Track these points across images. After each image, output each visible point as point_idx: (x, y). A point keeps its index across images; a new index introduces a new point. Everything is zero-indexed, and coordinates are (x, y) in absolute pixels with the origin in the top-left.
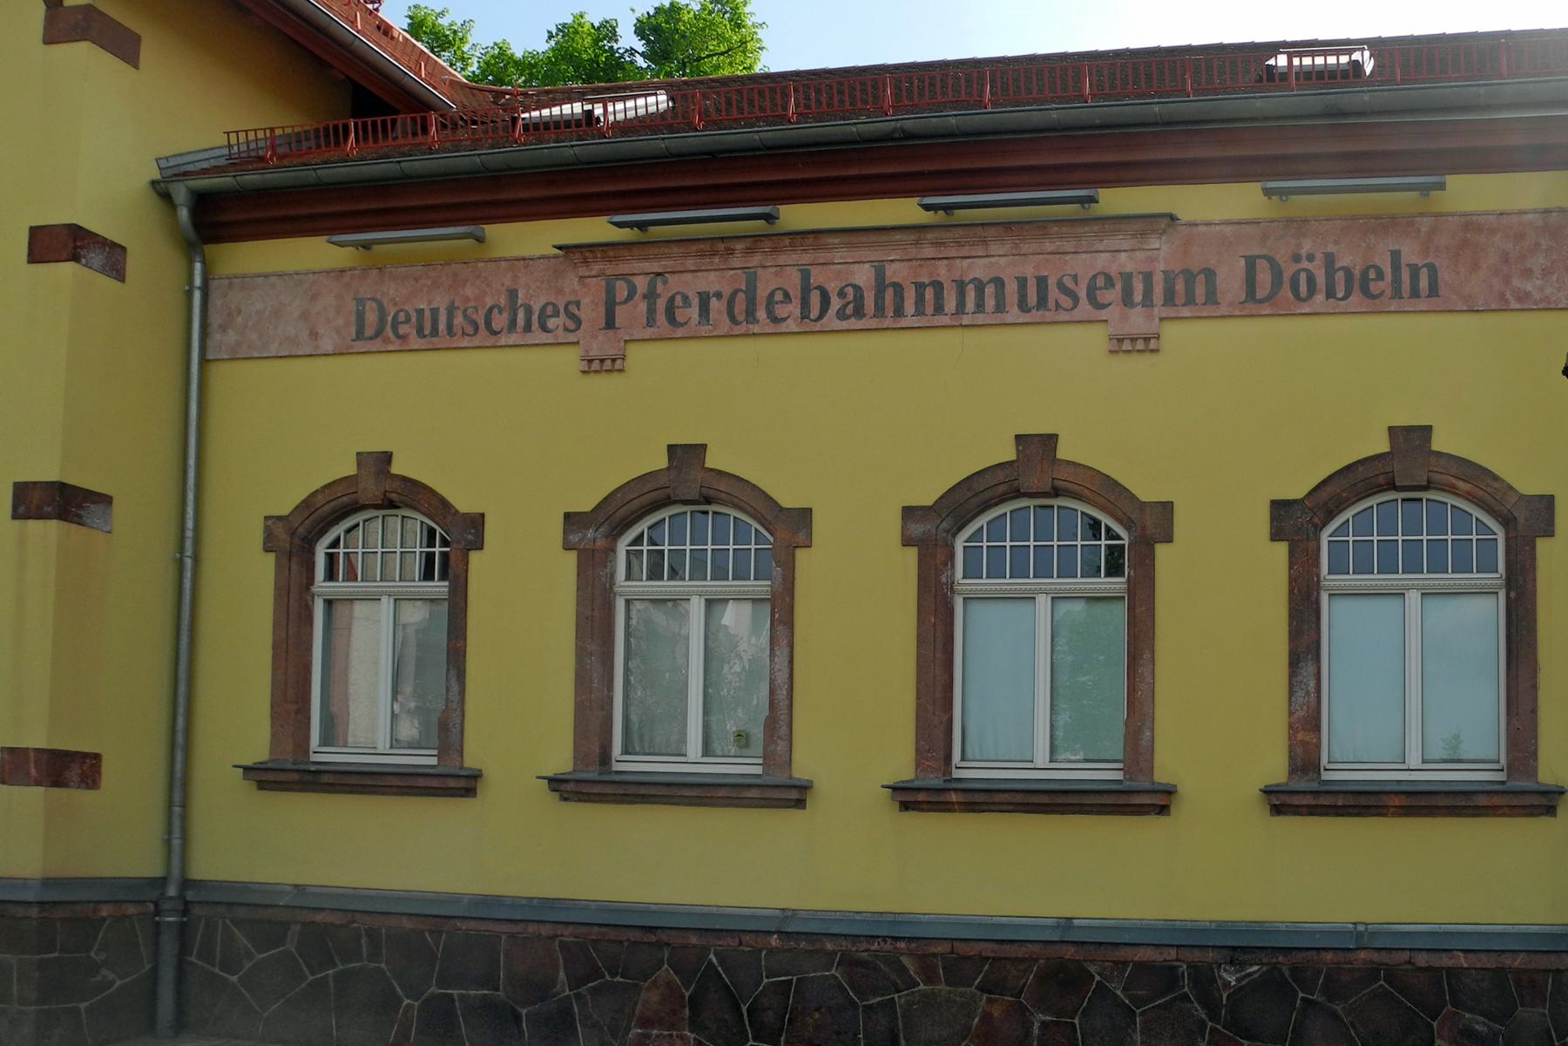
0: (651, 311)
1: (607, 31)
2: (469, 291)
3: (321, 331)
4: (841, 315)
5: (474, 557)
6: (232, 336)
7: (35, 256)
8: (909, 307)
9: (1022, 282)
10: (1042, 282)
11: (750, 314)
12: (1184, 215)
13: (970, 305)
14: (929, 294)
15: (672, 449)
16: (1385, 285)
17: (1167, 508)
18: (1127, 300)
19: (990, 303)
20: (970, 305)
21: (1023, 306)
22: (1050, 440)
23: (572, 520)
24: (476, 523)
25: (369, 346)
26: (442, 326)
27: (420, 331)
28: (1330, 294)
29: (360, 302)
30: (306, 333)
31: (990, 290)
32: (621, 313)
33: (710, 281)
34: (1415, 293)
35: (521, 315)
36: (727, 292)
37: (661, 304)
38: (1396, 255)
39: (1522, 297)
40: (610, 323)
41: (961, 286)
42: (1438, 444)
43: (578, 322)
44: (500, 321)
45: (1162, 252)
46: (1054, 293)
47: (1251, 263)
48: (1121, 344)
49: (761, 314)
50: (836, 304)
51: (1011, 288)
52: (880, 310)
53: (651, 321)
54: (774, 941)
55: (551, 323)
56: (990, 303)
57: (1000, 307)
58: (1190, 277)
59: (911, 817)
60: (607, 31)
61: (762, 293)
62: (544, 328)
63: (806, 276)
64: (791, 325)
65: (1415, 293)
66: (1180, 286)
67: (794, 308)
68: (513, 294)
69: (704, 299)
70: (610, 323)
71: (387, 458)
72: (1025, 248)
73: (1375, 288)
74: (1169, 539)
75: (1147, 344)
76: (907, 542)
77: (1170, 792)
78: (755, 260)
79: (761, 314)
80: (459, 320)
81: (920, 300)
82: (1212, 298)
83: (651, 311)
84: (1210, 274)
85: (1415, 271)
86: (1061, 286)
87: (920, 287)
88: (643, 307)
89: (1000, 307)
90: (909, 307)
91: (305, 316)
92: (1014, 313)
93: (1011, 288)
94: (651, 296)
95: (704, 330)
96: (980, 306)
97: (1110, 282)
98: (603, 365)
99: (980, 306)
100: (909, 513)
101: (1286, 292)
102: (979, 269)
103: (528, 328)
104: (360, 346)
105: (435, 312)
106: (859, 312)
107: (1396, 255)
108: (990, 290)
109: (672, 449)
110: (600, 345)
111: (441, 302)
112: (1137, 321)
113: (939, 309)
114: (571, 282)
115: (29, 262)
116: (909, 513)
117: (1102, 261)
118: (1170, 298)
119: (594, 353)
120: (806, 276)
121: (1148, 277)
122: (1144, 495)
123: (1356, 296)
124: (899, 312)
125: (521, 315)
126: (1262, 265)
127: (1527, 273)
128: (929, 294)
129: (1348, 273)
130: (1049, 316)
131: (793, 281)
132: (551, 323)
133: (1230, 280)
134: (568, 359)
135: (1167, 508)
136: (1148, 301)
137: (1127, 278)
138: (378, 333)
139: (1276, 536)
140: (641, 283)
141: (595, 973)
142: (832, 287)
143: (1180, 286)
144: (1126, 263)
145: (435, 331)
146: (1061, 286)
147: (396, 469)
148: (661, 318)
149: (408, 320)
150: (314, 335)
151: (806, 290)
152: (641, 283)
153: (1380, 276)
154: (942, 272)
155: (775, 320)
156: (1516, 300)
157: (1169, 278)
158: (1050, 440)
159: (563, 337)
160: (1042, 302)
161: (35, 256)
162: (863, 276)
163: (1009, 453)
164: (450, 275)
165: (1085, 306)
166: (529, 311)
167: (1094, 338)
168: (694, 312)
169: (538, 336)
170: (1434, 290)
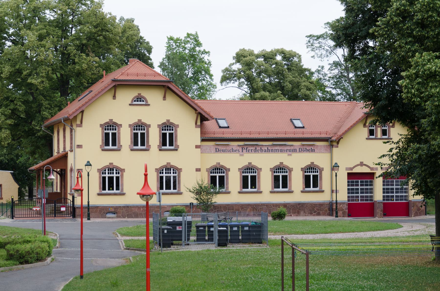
2: (228, 148)
7: (196, 148)
8: (270, 151)
10: (282, 150)
11: (256, 152)
12: (294, 145)
15: (249, 163)
18: (289, 151)
22: (282, 163)
29: (216, 148)
32: (243, 151)
33: (252, 148)
40: (242, 152)
42: (252, 164)
45: (292, 148)
46: (283, 151)
48: (289, 155)
51: (279, 150)
52: (268, 152)
53: (246, 152)
57: (278, 152)
58: (294, 149)
59: (271, 194)
61: (257, 150)
67: (260, 151)
68: (232, 148)
69: (251, 150)
70: (242, 152)
72: (421, 223)
75: (291, 155)
77: (324, 191)
78: (256, 147)
80: (227, 151)
82: (296, 151)
89: (278, 152)
90: (270, 151)
91: (210, 149)
92: (279, 152)
93: (279, 150)
94: (246, 149)
98: (241, 155)
100: (270, 168)
106: (266, 152)
109: (249, 163)
110: (242, 153)
111: (225, 149)
112: (290, 153)
118: (293, 151)
126: (300, 149)
131: (260, 149)
133: (298, 150)
134: (238, 155)
136: (291, 151)
137: (289, 150)
139: (301, 171)
141: (243, 208)
142: (263, 149)
144: (289, 148)
150: (211, 151)
152: (245, 148)
154: (273, 148)
156: (207, 71)
157: (293, 150)
158: (282, 163)
160: (282, 151)
161: (196, 148)
162: (266, 149)
163: (279, 164)
164: (17, 67)
168: (251, 151)
169: (235, 152)
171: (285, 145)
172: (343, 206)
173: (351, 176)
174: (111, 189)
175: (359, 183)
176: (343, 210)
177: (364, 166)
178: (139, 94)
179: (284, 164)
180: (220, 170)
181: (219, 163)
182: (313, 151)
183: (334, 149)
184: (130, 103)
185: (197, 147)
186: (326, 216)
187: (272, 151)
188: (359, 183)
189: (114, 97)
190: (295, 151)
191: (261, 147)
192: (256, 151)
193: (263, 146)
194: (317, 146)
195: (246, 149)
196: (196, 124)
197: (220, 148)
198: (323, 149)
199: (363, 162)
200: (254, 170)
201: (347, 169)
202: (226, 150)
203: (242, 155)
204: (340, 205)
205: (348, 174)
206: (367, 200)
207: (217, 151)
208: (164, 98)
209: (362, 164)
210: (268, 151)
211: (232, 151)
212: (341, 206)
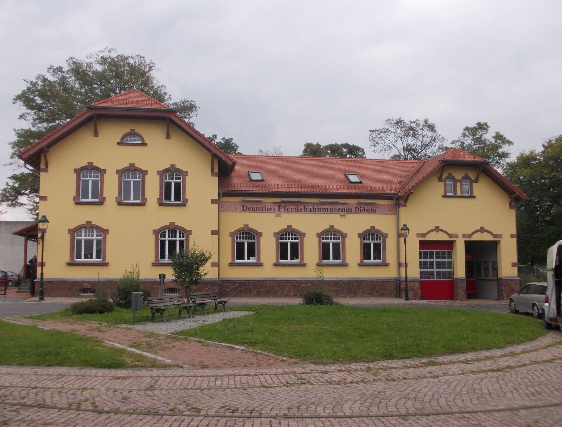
0: (285, 209)
1: (321, 146)
2: (259, 206)
3: (237, 209)
4: (309, 211)
5: (261, 237)
6: (223, 209)
8: (317, 211)
9: (330, 209)
10: (332, 209)
11: (298, 211)
13: (324, 211)
14: (319, 210)
16: (370, 211)
17: (347, 234)
19: (326, 211)
20: (324, 211)
21: (330, 212)
23: (275, 233)
24: (304, 234)
25: (245, 211)
26: (255, 210)
27: (252, 210)
28: (364, 212)
30: (235, 209)
31: (326, 209)
33: (292, 207)
34: (373, 212)
35: (267, 209)
36: (294, 208)
37: (286, 209)
38: (371, 208)
39: (385, 213)
40: (279, 211)
41: (323, 209)
43: (275, 210)
44: (264, 209)
45: (346, 207)
46: (334, 210)
47: (355, 208)
48: (341, 216)
49: (299, 211)
50: (308, 210)
51: (329, 210)
52: (313, 211)
53: (285, 211)
54: (303, 281)
55: (271, 210)
56: (326, 211)
57: (328, 211)
60: (321, 146)
61: (299, 208)
62: (270, 211)
63: (304, 207)
64: (303, 212)
65: (373, 212)
66: (348, 210)
67: (303, 210)
68: (266, 206)
69: (292, 208)
70: (279, 211)
71: (248, 225)
73: (369, 211)
74: (347, 237)
75: (344, 216)
76: (317, 237)
79: (299, 211)
80: (258, 209)
81: (318, 210)
83: (285, 209)
84: (351, 209)
85: (373, 210)
86: (335, 210)
87: (318, 209)
88: (284, 209)
90: (317, 211)
91: (235, 207)
93: (329, 210)
94: (285, 208)
95: (292, 212)
96: (325, 211)
97: (340, 209)
98: (277, 216)
99: (325, 211)
100: (317, 234)
101: (359, 211)
102: (325, 207)
103: (268, 210)
104: (243, 211)
105: (254, 208)
106: (311, 211)
107: (371, 208)
108: (326, 209)
112: (343, 214)
113: (320, 211)
114: (274, 206)
115: (512, 266)
116: (317, 234)
117: (339, 207)
119: (277, 214)
120: (304, 207)
121: (344, 209)
122: (344, 232)
123: (367, 212)
124: (316, 211)
125: (267, 209)
127: (385, 210)
128: (319, 210)
129: (366, 210)
130: (333, 213)
131: (303, 208)
132: (271, 210)
133: (353, 210)
134: (273, 215)
135: (347, 234)
136: (344, 212)
137: (342, 209)
138: (246, 210)
140: (283, 207)
142: (308, 208)
143: (348, 210)
145: (254, 210)
146: (335, 210)
147: (249, 227)
148: (286, 210)
149: (302, 209)
150: (236, 210)
151: (304, 208)
152: (283, 207)
153: (302, 209)
155: (300, 211)
159: (273, 212)
160: (333, 211)
162: (311, 207)
165: (337, 212)
166: (268, 209)
167: (338, 216)
168: (290, 210)
169: (269, 212)
170: (375, 212)
171: (337, 203)
172: (414, 284)
173: (425, 245)
174: (89, 256)
175: (435, 255)
176: (414, 290)
177: (440, 232)
178: (133, 131)
179: (335, 228)
180: (249, 235)
181: (248, 225)
182: (373, 211)
183: (402, 209)
184: (119, 142)
185: (213, 201)
186: (392, 297)
187: (320, 211)
188: (435, 255)
189: (96, 134)
190: (349, 211)
191: (304, 205)
192: (297, 210)
193: (306, 203)
194: (379, 205)
195: (285, 208)
196: (212, 170)
197: (248, 205)
198: (386, 209)
199: (438, 227)
200: (251, 234)
201: (418, 235)
202: (257, 208)
203: (279, 216)
204: (410, 284)
205: (421, 242)
206: (445, 277)
207: (245, 209)
208: (168, 137)
209: (437, 229)
210: (313, 210)
211: (266, 210)
212: (411, 284)
